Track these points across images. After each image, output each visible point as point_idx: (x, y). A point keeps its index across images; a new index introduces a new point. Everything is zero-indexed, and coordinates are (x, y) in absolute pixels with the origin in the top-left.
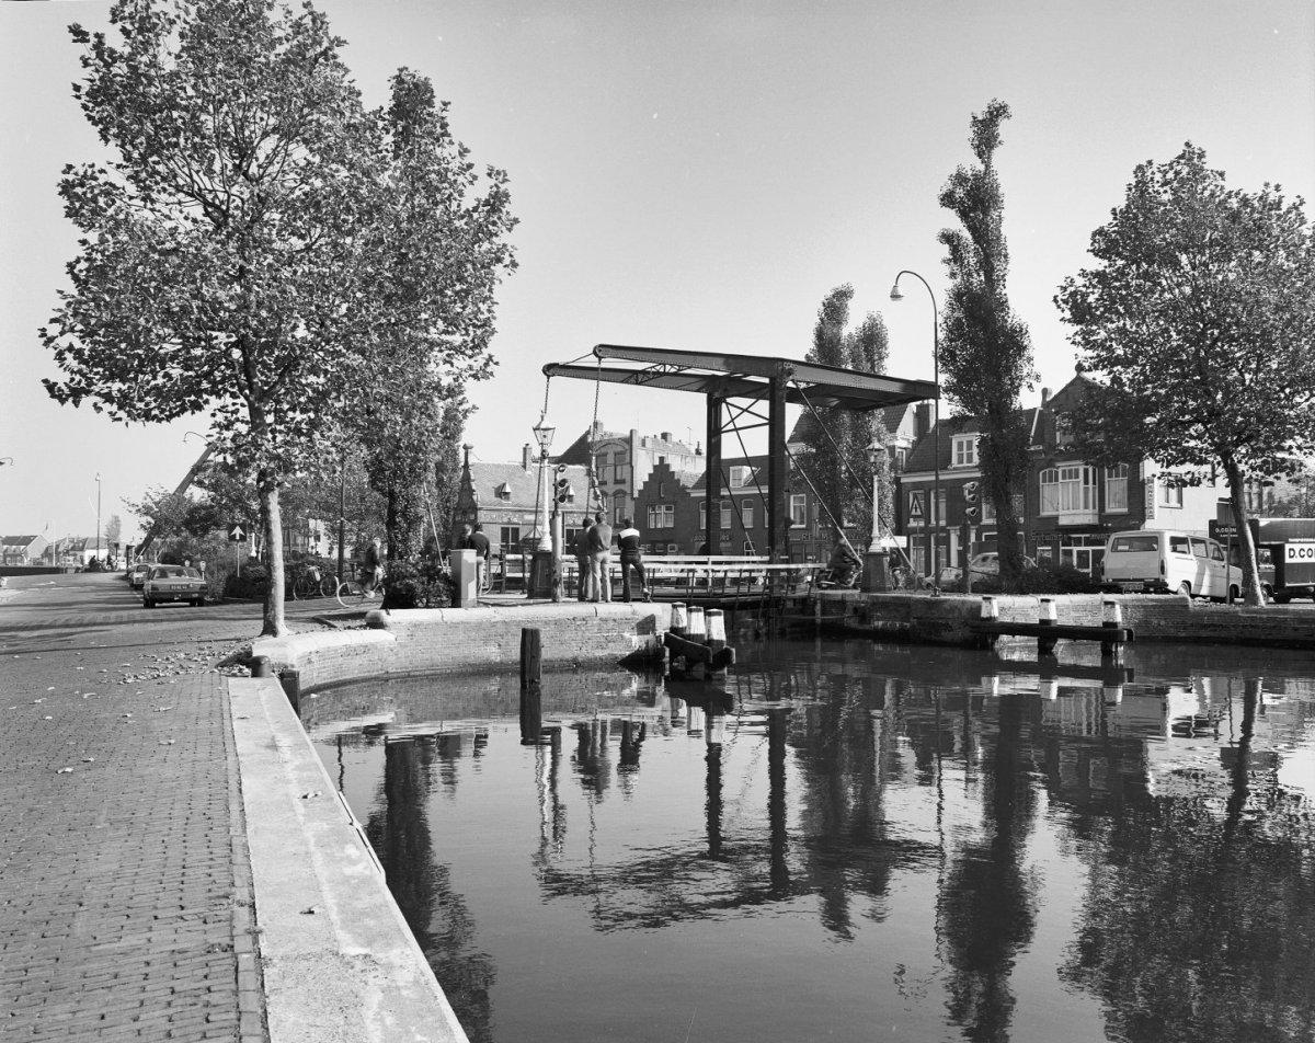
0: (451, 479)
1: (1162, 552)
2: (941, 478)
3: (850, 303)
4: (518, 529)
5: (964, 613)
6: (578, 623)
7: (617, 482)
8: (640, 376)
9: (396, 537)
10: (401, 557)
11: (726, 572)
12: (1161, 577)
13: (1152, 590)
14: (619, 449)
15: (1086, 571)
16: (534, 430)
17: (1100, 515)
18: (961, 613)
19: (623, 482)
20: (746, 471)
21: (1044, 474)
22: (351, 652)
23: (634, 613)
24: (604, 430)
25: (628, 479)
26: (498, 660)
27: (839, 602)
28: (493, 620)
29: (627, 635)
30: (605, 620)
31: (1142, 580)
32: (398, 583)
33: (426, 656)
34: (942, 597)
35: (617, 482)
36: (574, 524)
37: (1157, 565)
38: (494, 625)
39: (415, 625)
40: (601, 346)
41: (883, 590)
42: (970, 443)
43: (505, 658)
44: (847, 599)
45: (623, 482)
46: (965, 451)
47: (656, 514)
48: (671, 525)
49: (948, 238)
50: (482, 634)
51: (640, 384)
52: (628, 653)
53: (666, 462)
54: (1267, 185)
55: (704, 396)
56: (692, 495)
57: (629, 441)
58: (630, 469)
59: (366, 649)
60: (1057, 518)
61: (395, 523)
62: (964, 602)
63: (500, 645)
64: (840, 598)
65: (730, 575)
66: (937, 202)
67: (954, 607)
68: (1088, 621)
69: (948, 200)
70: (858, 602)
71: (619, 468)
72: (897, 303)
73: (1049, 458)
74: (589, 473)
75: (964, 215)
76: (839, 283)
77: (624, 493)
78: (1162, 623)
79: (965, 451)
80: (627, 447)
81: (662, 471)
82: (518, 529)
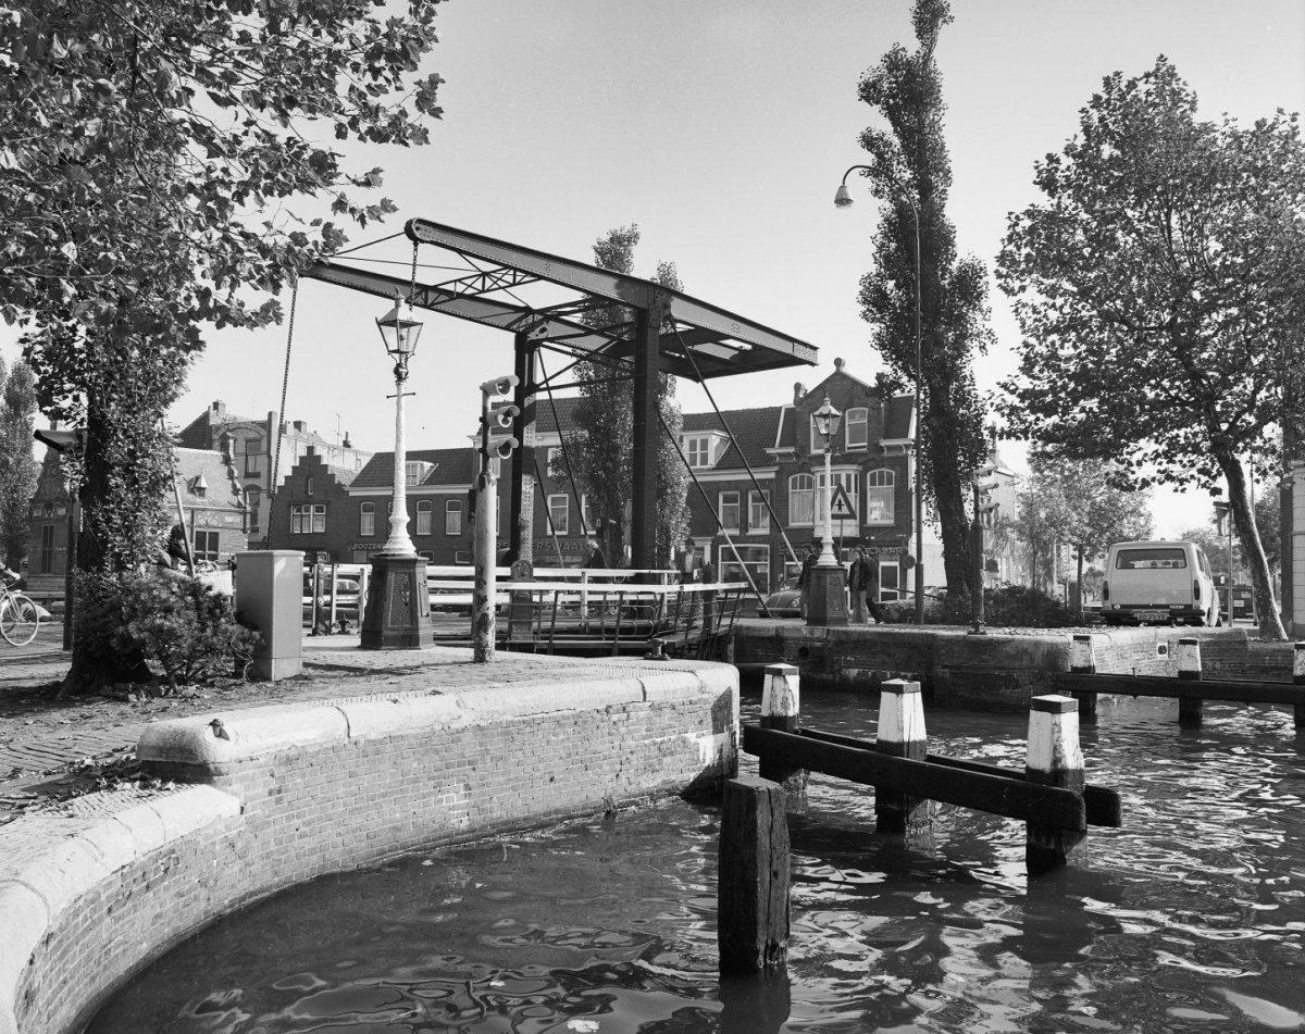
0: (19, 462)
1: (1192, 570)
2: (756, 477)
3: (634, 249)
4: (217, 534)
5: (1038, 660)
6: (615, 718)
7: (248, 475)
8: (432, 296)
9: (109, 520)
10: (120, 567)
11: (557, 593)
12: (1195, 603)
13: (1180, 620)
14: (252, 435)
15: (884, 590)
16: (380, 324)
17: (861, 528)
18: (1032, 660)
19: (257, 475)
20: (715, 439)
21: (794, 480)
22: (139, 881)
23: (702, 689)
24: (227, 412)
25: (264, 473)
26: (464, 825)
27: (770, 639)
28: (455, 726)
29: (691, 737)
30: (656, 708)
31: (1167, 606)
32: (132, 627)
33: (310, 843)
34: (995, 633)
35: (248, 475)
36: (207, 525)
37: (1189, 587)
38: (456, 736)
39: (289, 761)
40: (420, 221)
41: (843, 621)
42: (705, 444)
43: (478, 819)
44: (786, 634)
45: (257, 475)
46: (698, 451)
47: (302, 516)
48: (320, 529)
49: (869, 141)
50: (433, 761)
51: (429, 308)
52: (692, 776)
53: (317, 453)
54: (1280, 111)
55: (509, 338)
56: (351, 494)
57: (267, 425)
58: (266, 460)
59: (169, 861)
60: (812, 529)
61: (106, 489)
62: (1037, 644)
63: (468, 787)
64: (773, 633)
65: (562, 598)
66: (855, 94)
67: (1023, 651)
68: (1150, 666)
69: (869, 92)
70: (806, 639)
71: (251, 459)
72: (844, 210)
73: (801, 461)
74: (227, 461)
75: (893, 114)
76: (622, 225)
77: (258, 489)
78: (1218, 666)
79: (698, 451)
80: (264, 433)
81: (310, 465)
82: (217, 534)
